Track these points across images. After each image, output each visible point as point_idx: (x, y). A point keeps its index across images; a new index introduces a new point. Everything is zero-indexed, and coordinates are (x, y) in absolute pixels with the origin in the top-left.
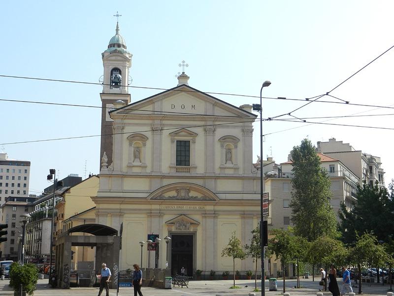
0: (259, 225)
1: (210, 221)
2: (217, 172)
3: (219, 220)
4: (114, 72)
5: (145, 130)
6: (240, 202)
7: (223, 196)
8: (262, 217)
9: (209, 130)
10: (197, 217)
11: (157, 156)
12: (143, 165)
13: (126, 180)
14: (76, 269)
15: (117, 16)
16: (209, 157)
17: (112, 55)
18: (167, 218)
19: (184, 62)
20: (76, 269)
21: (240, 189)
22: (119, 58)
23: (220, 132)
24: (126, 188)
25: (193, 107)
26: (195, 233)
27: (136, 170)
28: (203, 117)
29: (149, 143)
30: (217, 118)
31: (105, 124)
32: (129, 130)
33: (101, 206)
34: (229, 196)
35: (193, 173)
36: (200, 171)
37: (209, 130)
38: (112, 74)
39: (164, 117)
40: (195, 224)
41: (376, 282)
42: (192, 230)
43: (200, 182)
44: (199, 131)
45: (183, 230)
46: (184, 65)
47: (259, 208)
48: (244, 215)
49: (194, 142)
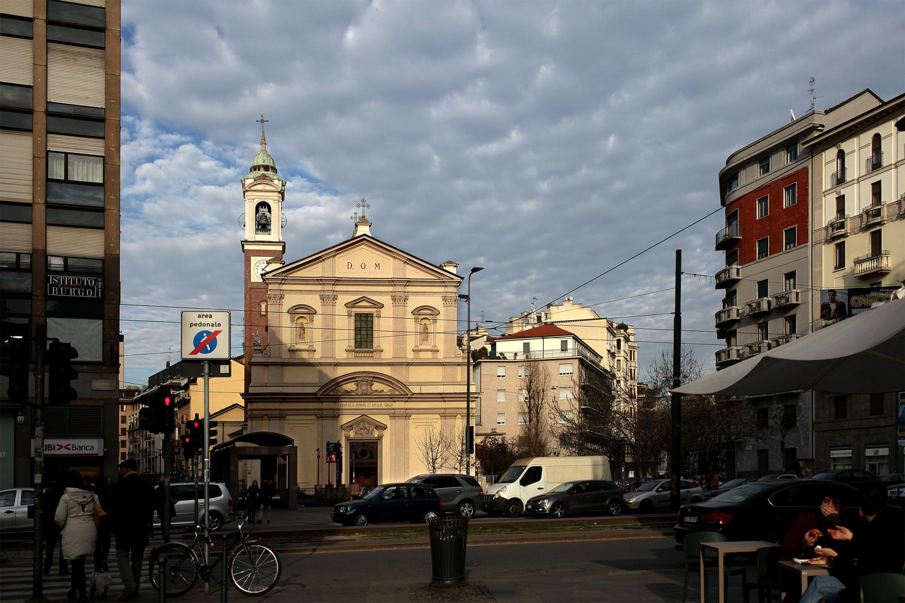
0: (464, 447)
1: (400, 422)
2: (410, 356)
3: (286, 422)
4: (261, 209)
5: (313, 301)
6: (442, 397)
7: (415, 389)
8: (468, 421)
9: (400, 300)
10: (383, 419)
11: (329, 330)
12: (311, 348)
13: (288, 370)
14: (19, 492)
15: (262, 121)
16: (400, 334)
17: (259, 181)
19: (623, 327)
20: (19, 492)
22: (268, 188)
23: (415, 302)
24: (287, 380)
25: (377, 265)
26: (380, 438)
27: (428, 356)
28: (391, 282)
29: (318, 320)
31: (249, 286)
32: (290, 301)
33: (255, 406)
34: (426, 389)
35: (376, 358)
36: (388, 355)
37: (400, 300)
38: (257, 211)
39: (338, 281)
41: (412, 489)
42: (376, 434)
43: (386, 371)
44: (386, 300)
45: (365, 436)
46: (363, 206)
47: (465, 405)
48: (445, 415)
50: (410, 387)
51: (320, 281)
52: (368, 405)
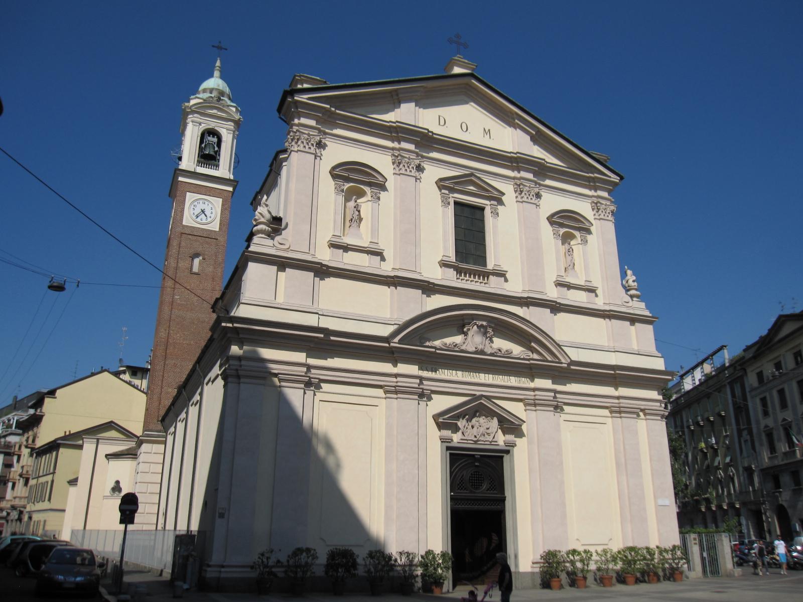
5: (381, 162)
7: (576, 355)
10: (517, 409)
11: (410, 232)
18: (441, 403)
21: (604, 342)
23: (552, 202)
30: (541, 170)
35: (494, 285)
36: (515, 287)
40: (511, 426)
42: (501, 440)
44: (508, 189)
51: (398, 132)
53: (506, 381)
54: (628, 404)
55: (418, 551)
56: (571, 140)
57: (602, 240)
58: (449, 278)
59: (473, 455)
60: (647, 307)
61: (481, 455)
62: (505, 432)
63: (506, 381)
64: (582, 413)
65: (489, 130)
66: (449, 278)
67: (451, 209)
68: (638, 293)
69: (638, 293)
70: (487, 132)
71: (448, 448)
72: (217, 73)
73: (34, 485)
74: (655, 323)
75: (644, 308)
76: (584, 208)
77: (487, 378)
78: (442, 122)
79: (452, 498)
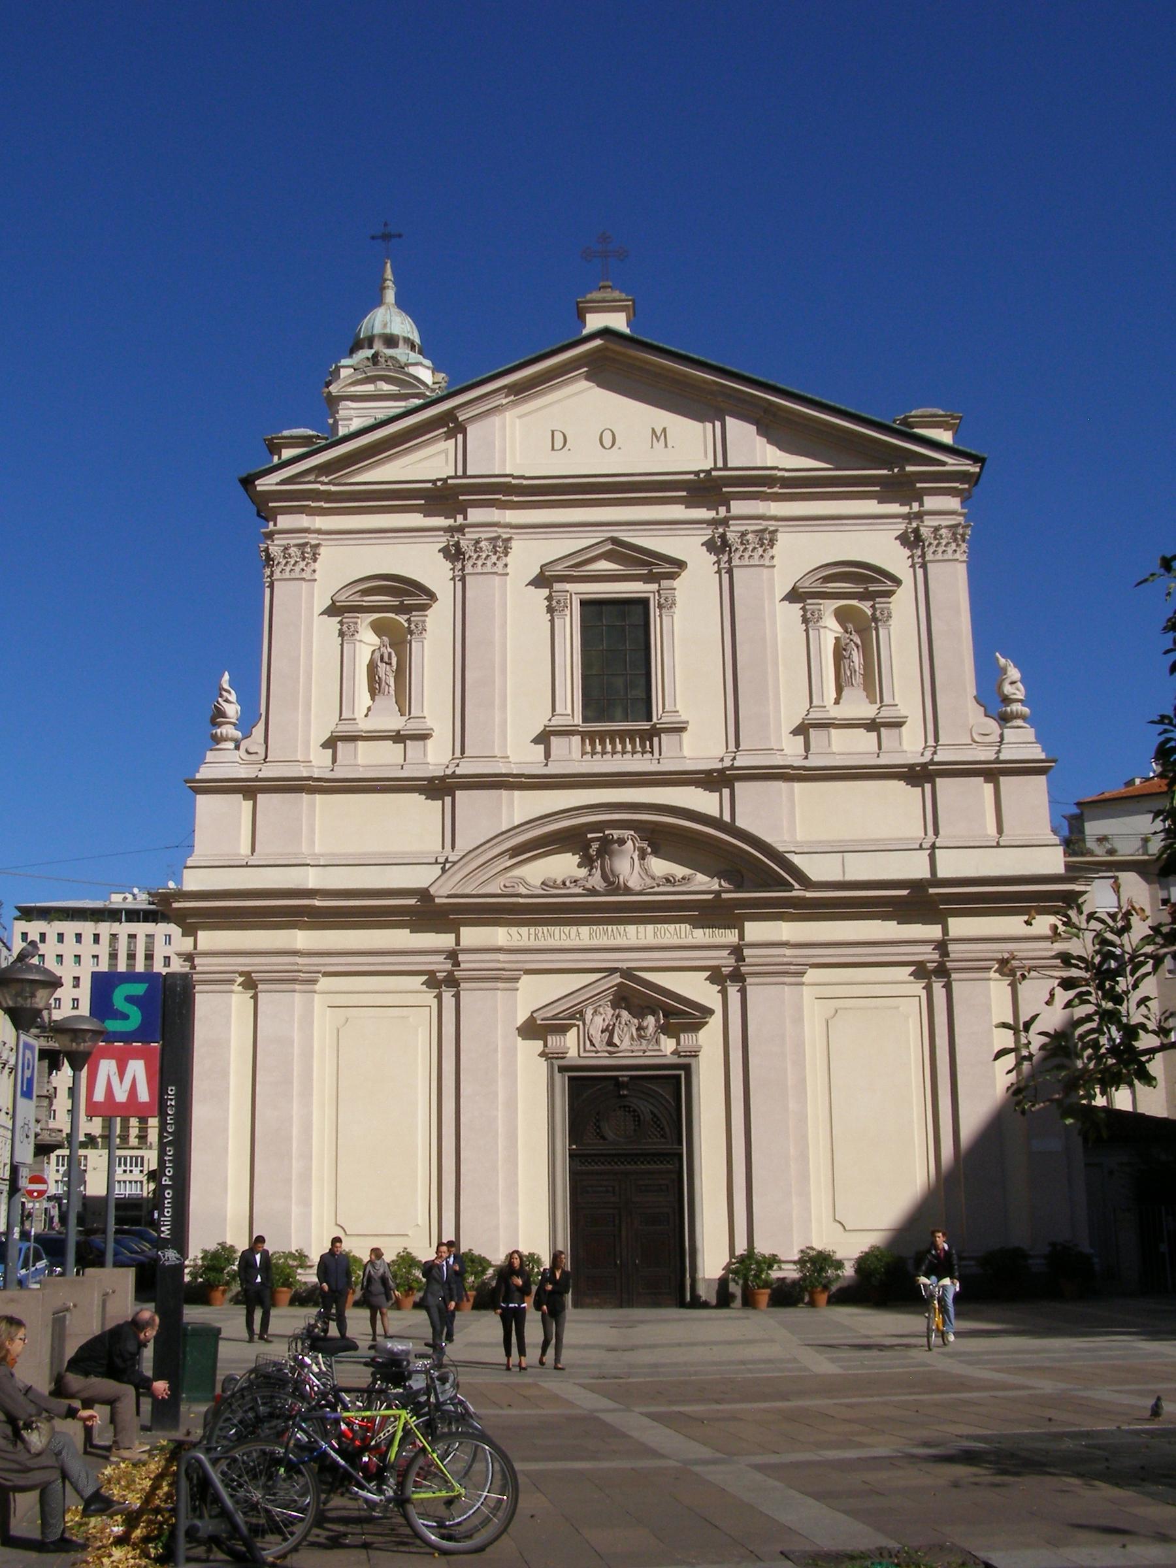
5: (422, 562)
10: (695, 987)
23: (801, 552)
28: (705, 489)
30: (761, 483)
40: (683, 1017)
49: (667, 605)
50: (796, 860)
51: (443, 498)
52: (634, 934)
53: (683, 935)
54: (980, 951)
55: (875, 1233)
56: (843, 408)
57: (934, 610)
58: (570, 756)
59: (616, 1077)
60: (1039, 739)
61: (631, 1077)
62: (667, 1030)
63: (683, 935)
64: (873, 979)
65: (664, 430)
66: (570, 756)
67: (570, 625)
68: (1026, 710)
69: (1026, 710)
70: (659, 435)
71: (562, 1069)
72: (390, 296)
73: (660, 1050)
74: (1052, 771)
75: (1034, 740)
76: (880, 547)
77: (641, 935)
78: (559, 443)
79: (573, 1156)
